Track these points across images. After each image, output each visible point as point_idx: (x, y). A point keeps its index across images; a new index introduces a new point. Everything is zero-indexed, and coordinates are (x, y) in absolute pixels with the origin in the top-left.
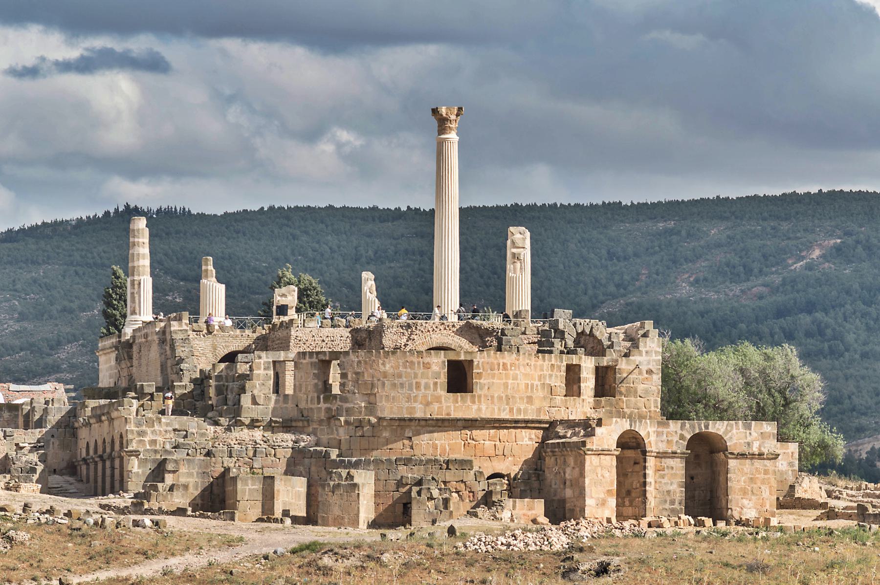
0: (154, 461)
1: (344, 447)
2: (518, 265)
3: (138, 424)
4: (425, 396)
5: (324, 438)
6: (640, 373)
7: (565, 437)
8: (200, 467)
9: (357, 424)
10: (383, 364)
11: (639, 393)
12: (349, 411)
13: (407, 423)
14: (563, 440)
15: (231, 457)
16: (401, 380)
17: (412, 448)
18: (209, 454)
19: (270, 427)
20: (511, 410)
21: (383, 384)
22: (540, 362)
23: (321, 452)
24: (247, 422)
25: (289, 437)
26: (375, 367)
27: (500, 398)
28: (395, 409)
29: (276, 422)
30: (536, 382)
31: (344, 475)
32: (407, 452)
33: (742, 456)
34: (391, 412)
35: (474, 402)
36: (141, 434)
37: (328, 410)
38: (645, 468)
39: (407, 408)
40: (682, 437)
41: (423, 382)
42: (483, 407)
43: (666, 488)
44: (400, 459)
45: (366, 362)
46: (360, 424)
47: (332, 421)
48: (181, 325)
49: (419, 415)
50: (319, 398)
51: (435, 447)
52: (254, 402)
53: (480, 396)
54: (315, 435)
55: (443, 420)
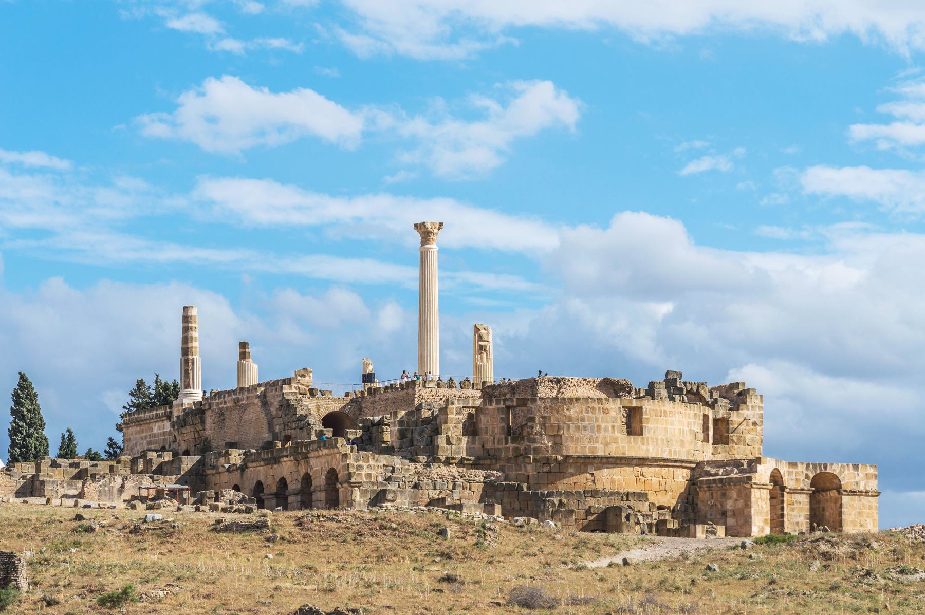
0: (373, 491)
1: (532, 481)
2: (484, 355)
3: (357, 460)
4: (605, 438)
5: (512, 474)
6: (748, 425)
7: (717, 474)
8: (411, 498)
9: (544, 462)
10: (568, 409)
12: (536, 451)
13: (591, 461)
14: (717, 477)
15: (435, 489)
16: (584, 424)
17: (594, 482)
18: (416, 486)
19: (461, 463)
20: (670, 451)
21: (569, 427)
22: (688, 411)
23: (514, 486)
24: (443, 459)
25: (481, 473)
26: (561, 411)
27: (662, 440)
28: (579, 449)
29: (468, 460)
30: (686, 428)
31: (557, 503)
32: (590, 486)
33: (853, 493)
34: (576, 451)
35: (643, 444)
36: (360, 468)
37: (516, 449)
38: (783, 502)
39: (590, 448)
40: (807, 477)
41: (603, 425)
42: (650, 448)
43: (795, 520)
44: (588, 492)
45: (552, 407)
46: (547, 461)
47: (521, 459)
48: (291, 387)
49: (600, 453)
51: (613, 482)
52: (449, 442)
53: (648, 438)
54: (503, 471)
55: (621, 458)
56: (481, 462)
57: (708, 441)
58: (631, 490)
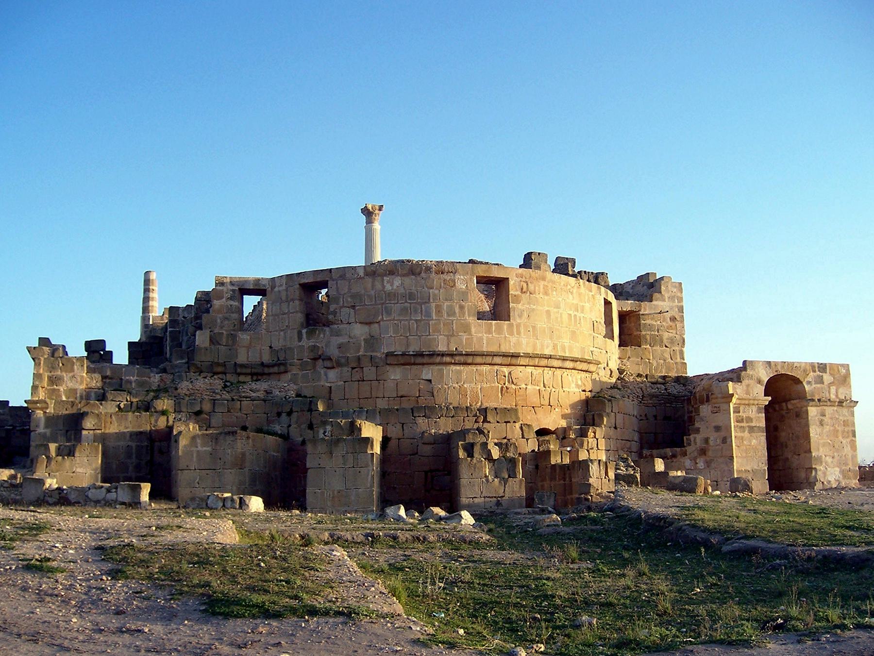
11: (665, 341)
35: (512, 334)
42: (524, 341)
50: (300, 334)
53: (518, 326)
56: (266, 370)
57: (612, 338)
58: (492, 404)
